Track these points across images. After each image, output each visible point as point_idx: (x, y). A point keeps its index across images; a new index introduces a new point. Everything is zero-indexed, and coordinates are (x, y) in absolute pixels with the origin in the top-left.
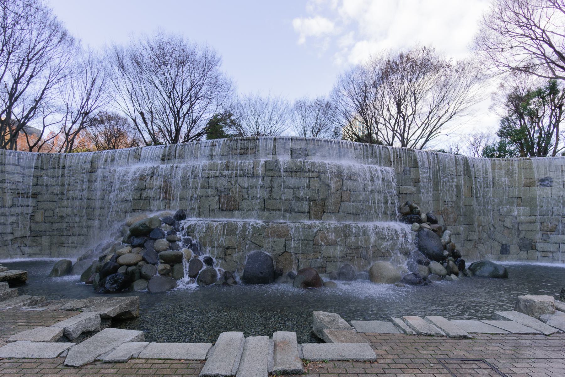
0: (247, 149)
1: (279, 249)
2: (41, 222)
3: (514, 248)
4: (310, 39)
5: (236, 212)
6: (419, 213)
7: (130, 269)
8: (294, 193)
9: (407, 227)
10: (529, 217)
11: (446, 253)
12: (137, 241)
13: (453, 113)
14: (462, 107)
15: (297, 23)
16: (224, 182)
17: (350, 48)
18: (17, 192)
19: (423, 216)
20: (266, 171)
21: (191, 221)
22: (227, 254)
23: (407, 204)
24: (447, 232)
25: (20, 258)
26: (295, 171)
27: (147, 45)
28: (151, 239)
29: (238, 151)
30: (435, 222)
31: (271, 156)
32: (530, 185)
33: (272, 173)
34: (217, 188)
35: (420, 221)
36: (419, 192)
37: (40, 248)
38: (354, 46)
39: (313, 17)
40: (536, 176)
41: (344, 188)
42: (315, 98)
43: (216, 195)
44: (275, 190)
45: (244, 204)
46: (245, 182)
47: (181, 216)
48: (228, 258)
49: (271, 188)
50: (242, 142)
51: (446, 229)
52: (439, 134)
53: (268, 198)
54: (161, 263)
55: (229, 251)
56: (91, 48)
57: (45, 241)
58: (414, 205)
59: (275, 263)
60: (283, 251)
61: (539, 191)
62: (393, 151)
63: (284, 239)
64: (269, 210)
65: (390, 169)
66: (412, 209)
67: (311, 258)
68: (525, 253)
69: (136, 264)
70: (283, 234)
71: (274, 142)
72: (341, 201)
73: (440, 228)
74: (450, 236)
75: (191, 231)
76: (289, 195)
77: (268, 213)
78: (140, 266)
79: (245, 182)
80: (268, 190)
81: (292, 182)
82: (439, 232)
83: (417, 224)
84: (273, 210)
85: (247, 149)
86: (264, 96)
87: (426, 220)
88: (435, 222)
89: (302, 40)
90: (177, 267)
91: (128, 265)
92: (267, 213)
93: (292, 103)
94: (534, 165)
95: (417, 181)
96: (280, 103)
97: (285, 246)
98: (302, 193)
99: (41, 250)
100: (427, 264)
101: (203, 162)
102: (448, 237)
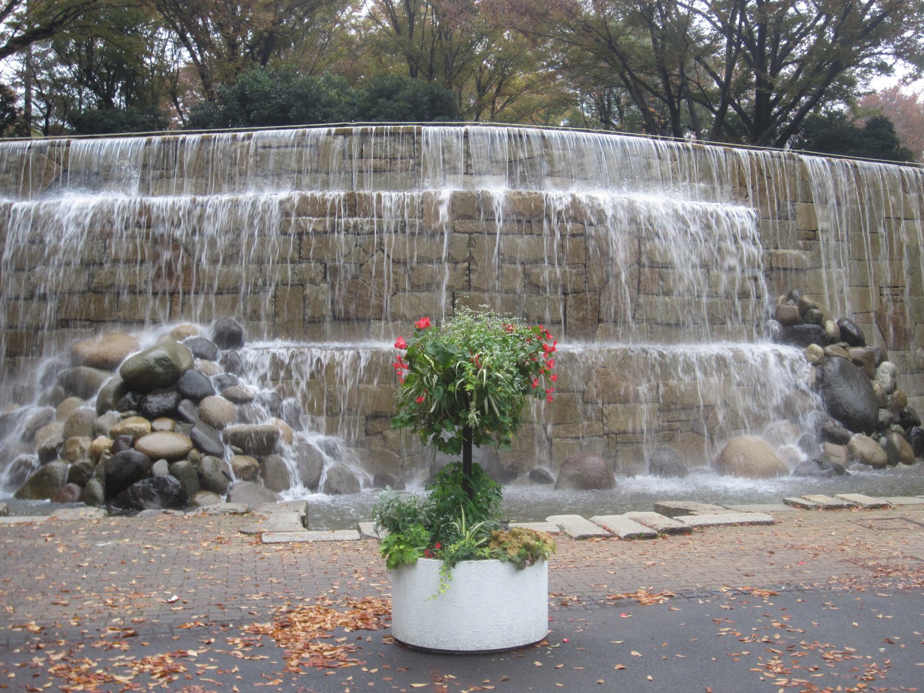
6: (819, 321)
9: (790, 351)
19: (831, 327)
30: (857, 341)
33: (470, 225)
35: (826, 341)
51: (883, 358)
58: (806, 299)
62: (751, 159)
66: (804, 309)
74: (893, 375)
90: (271, 460)
95: (811, 236)
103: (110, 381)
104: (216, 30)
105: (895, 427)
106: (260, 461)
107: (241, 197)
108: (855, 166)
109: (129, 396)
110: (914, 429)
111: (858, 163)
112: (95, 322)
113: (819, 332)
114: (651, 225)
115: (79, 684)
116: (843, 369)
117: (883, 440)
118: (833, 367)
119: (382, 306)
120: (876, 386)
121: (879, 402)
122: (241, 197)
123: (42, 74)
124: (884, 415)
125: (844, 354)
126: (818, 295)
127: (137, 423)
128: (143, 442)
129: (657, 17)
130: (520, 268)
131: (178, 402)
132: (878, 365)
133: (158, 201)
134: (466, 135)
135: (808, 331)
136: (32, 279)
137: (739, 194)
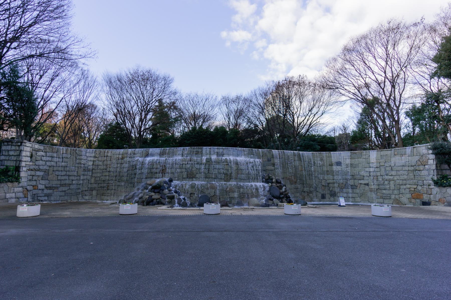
0: (198, 152)
1: (212, 194)
2: (93, 183)
3: (327, 196)
4: (235, 44)
5: (194, 179)
7: (158, 200)
8: (218, 171)
9: (266, 185)
10: (333, 181)
11: (282, 196)
12: (156, 191)
13: (323, 112)
14: (328, 108)
15: (224, 34)
16: (188, 166)
17: (265, 48)
20: (207, 162)
21: (175, 183)
22: (191, 196)
26: (218, 162)
27: (129, 74)
28: (161, 190)
29: (195, 153)
31: (209, 155)
33: (209, 163)
34: (186, 169)
35: (272, 183)
37: (91, 196)
38: (267, 47)
39: (236, 30)
41: (239, 168)
42: (236, 95)
43: (186, 171)
45: (197, 176)
46: (197, 166)
47: (171, 181)
48: (191, 198)
49: (209, 169)
50: (196, 149)
52: (319, 123)
53: (207, 173)
54: (167, 199)
55: (192, 195)
56: (68, 50)
57: (94, 193)
59: (210, 199)
60: (213, 195)
62: (262, 152)
63: (214, 190)
64: (208, 178)
68: (333, 198)
69: (159, 199)
70: (213, 187)
71: (210, 150)
72: (238, 174)
75: (176, 186)
76: (216, 171)
77: (208, 179)
78: (160, 200)
79: (197, 166)
80: (207, 170)
81: (218, 166)
82: (281, 188)
83: (270, 184)
84: (210, 178)
85: (198, 152)
86: (200, 93)
87: (276, 182)
89: (228, 44)
90: (173, 200)
91: (157, 199)
92: (207, 179)
93: (219, 98)
94: (332, 156)
95: (274, 165)
96: (211, 97)
97: (214, 193)
99: (92, 197)
100: (272, 200)
101: (180, 157)
103: (150, 187)
104: (254, 137)
106: (171, 200)
107: (158, 158)
108: (284, 152)
109: (153, 190)
110: (166, 196)
111: (284, 151)
112: (151, 178)
121: (281, 194)
122: (158, 158)
127: (153, 194)
128: (153, 197)
129: (60, 116)
130: (217, 170)
131: (160, 191)
132: (283, 187)
133: (161, 159)
134: (210, 148)
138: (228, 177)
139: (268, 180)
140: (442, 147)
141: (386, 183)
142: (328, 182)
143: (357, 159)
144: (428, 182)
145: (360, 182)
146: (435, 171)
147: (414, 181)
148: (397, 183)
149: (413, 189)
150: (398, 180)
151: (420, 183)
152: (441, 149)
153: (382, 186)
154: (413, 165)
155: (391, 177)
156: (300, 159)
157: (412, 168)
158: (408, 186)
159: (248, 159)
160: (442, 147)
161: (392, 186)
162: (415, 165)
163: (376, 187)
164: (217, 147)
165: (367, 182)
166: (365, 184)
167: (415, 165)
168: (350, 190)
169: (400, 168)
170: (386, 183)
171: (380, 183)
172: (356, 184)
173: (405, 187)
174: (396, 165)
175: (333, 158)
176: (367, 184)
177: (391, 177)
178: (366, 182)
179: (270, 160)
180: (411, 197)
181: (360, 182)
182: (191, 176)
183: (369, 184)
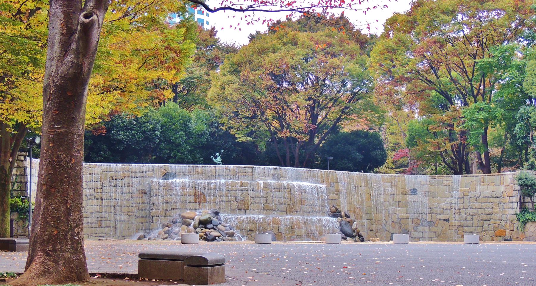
6: (340, 212)
9: (334, 220)
18: (386, 99)
19: (343, 214)
23: (333, 206)
24: (355, 223)
25: (6, 224)
30: (349, 217)
32: (404, 193)
35: (341, 217)
36: (339, 198)
40: (407, 186)
44: (270, 198)
51: (354, 221)
58: (337, 207)
61: (410, 198)
65: (323, 186)
66: (337, 209)
67: (118, 217)
73: (351, 221)
74: (357, 225)
81: (278, 194)
82: (351, 223)
87: (344, 216)
88: (349, 217)
94: (407, 180)
95: (338, 191)
98: (282, 201)
102: (355, 226)
105: (357, 237)
113: (340, 215)
114: (464, 149)
115: (40, 209)
116: (345, 224)
117: (354, 239)
118: (343, 223)
119: (32, 251)
120: (353, 227)
123: (187, 15)
124: (354, 234)
125: (346, 220)
126: (339, 206)
135: (337, 215)
136: (327, 46)
137: (322, 182)
138: (291, 209)
139: (336, 213)
140: (526, 178)
141: (469, 217)
142: (400, 217)
143: (436, 186)
144: (320, 221)
145: (439, 217)
146: (519, 203)
147: (498, 215)
148: (481, 218)
149: (496, 225)
150: (482, 214)
151: (504, 218)
152: (525, 180)
153: (464, 222)
154: (499, 196)
155: (475, 211)
156: (367, 185)
157: (497, 200)
158: (492, 221)
159: (313, 185)
160: (526, 178)
161: (475, 221)
162: (501, 197)
163: (457, 223)
164: (272, 167)
165: (448, 218)
166: (445, 220)
167: (501, 197)
168: (427, 229)
169: (484, 200)
170: (469, 217)
171: (462, 219)
172: (434, 220)
173: (488, 222)
174: (482, 196)
175: (407, 183)
176: (447, 220)
177: (475, 211)
178: (446, 217)
179: (332, 185)
180: (494, 234)
181: (439, 217)
182: (243, 207)
183: (450, 220)
